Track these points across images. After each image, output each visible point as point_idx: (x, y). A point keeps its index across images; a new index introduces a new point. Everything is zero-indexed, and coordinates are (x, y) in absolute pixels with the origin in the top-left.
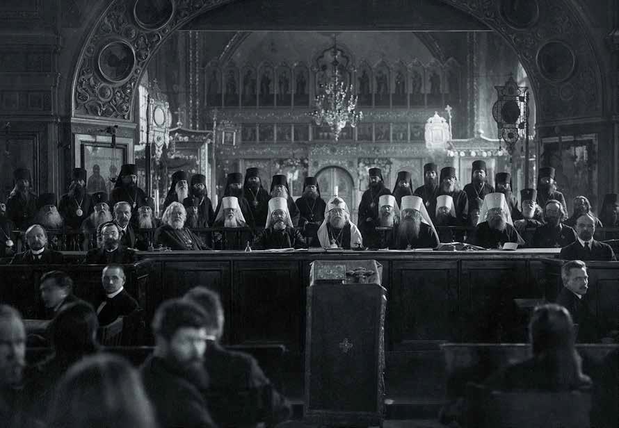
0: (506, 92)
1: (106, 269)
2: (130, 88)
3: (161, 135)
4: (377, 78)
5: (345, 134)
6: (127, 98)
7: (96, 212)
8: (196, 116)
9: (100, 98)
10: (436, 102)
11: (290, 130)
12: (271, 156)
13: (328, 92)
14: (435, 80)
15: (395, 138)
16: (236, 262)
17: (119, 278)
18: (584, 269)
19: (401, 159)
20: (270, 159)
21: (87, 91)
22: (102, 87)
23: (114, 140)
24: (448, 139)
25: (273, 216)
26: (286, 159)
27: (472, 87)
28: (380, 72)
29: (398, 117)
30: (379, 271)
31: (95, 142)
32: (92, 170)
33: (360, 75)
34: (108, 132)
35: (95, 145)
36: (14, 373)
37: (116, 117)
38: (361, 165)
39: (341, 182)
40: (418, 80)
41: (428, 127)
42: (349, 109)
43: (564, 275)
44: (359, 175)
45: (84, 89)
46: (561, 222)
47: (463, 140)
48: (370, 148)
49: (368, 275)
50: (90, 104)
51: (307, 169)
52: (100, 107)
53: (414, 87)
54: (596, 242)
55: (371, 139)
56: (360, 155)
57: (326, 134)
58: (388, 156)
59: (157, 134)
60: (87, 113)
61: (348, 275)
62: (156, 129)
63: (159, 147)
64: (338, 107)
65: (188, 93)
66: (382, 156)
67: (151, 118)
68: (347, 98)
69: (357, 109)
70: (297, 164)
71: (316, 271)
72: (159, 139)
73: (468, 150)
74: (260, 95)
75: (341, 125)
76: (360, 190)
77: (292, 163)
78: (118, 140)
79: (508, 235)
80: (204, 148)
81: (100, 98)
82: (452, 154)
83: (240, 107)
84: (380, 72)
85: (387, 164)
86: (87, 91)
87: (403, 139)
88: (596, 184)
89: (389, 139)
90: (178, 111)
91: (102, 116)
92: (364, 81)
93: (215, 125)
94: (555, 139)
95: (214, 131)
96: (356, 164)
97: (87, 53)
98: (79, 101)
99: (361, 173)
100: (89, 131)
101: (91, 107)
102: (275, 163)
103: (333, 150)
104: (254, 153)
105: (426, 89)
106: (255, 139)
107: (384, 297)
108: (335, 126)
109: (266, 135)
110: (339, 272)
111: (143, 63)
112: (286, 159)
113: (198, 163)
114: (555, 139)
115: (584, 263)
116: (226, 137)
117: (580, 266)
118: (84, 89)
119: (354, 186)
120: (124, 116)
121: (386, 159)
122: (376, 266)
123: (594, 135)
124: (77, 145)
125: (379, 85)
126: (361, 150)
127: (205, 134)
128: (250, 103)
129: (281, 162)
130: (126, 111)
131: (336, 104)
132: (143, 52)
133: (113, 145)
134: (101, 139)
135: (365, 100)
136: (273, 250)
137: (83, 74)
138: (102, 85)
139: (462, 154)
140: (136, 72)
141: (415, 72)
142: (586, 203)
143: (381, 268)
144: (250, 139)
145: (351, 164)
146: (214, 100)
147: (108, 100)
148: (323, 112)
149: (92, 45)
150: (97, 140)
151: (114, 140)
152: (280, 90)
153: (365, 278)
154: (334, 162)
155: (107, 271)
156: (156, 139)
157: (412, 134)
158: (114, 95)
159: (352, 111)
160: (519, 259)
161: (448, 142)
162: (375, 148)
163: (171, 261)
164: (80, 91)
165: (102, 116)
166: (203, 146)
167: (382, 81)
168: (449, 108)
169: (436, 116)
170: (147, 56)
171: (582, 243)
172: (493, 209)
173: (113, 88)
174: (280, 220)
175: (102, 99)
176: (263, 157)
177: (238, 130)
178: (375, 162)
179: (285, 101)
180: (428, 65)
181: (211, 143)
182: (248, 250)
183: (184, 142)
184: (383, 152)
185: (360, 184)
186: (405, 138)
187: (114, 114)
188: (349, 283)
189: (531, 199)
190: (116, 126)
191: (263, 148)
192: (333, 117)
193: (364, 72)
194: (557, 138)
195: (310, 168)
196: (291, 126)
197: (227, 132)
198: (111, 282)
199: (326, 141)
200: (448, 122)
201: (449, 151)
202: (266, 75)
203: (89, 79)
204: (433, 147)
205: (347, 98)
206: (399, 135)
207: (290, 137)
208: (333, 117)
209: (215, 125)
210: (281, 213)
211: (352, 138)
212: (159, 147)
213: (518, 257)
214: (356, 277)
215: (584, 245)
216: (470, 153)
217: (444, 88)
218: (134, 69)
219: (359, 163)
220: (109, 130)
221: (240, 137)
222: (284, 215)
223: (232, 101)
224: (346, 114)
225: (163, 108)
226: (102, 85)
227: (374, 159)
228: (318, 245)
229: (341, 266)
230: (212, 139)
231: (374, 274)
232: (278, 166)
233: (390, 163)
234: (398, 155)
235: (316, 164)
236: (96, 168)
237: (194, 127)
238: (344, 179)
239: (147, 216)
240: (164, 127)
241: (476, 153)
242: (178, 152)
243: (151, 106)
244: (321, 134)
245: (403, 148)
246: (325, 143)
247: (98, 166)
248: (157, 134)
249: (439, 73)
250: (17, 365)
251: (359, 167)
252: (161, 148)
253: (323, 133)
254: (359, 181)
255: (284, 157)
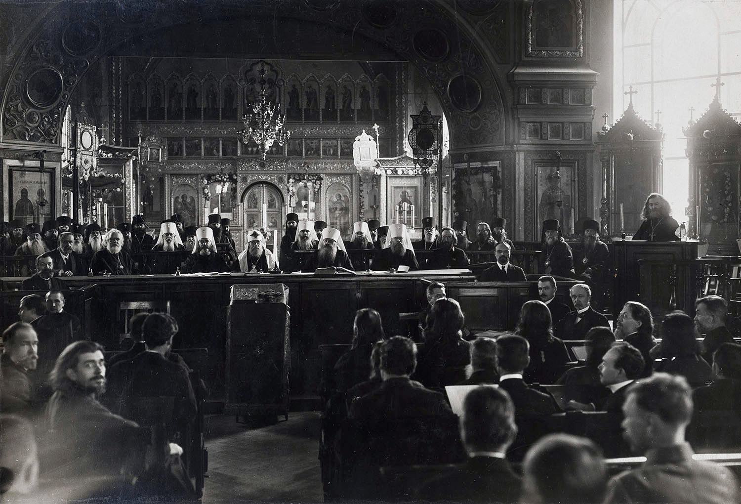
0: (420, 120)
1: (48, 294)
2: (58, 113)
3: (89, 158)
4: (307, 92)
5: (274, 149)
6: (55, 123)
7: (29, 241)
8: (119, 130)
9: (28, 123)
10: (366, 119)
11: (219, 144)
12: (198, 172)
13: (255, 111)
14: (365, 95)
15: (325, 152)
16: (16, 174)
17: (60, 301)
18: (443, 289)
19: (331, 175)
20: (197, 175)
21: (15, 117)
22: (30, 113)
23: (42, 164)
24: (376, 158)
25: (200, 243)
26: (214, 175)
27: (400, 102)
28: (310, 87)
29: (328, 133)
30: (286, 293)
31: (23, 167)
32: (20, 194)
33: (290, 89)
34: (36, 157)
35: (23, 169)
36: (32, 363)
37: (44, 141)
38: (291, 180)
39: (270, 198)
40: (348, 98)
41: (356, 145)
42: (277, 128)
43: (428, 294)
44: (288, 190)
45: (12, 115)
46: (454, 246)
47: (390, 159)
48: (299, 164)
49: (276, 295)
50: (18, 129)
51: (236, 185)
52: (28, 132)
53: (344, 103)
54: (511, 265)
55: (301, 154)
56: (290, 171)
57: (255, 149)
58: (318, 172)
59: (84, 158)
60: (15, 138)
61: (260, 296)
62: (83, 152)
63: (86, 170)
64: (266, 126)
65: (111, 106)
66: (313, 172)
67: (79, 142)
68: (275, 117)
69: (286, 126)
70: (225, 180)
71: (234, 294)
72: (86, 162)
73: (395, 168)
74: (186, 108)
75: (268, 144)
76: (290, 206)
77: (220, 179)
78: (46, 164)
79: (407, 259)
80: (129, 165)
81: (28, 123)
82: (378, 171)
83: (166, 120)
84: (310, 87)
85: (317, 180)
86: (15, 117)
87: (333, 154)
88: (500, 207)
89: (319, 155)
90: (101, 127)
91: (29, 140)
92: (294, 95)
93: (140, 141)
94: (464, 165)
95: (140, 148)
96: (285, 179)
97: (15, 80)
98: (7, 127)
99: (291, 189)
100: (17, 156)
101: (19, 132)
102: (202, 178)
103: (262, 165)
104: (180, 168)
105: (357, 104)
106: (181, 154)
107: (288, 312)
108: (263, 145)
109: (193, 150)
110: (253, 294)
111: (71, 88)
112: (214, 175)
113: (123, 181)
114: (464, 165)
115: (444, 285)
116: (151, 154)
117: (441, 287)
118: (12, 115)
119: (283, 201)
120: (52, 140)
121: (316, 174)
122: (284, 288)
123: (498, 162)
124: (6, 169)
125: (309, 100)
126: (292, 166)
127: (130, 151)
128: (175, 116)
129: (209, 177)
130: (54, 136)
131: (263, 123)
132: (71, 78)
133: (41, 169)
134: (28, 163)
135: (294, 115)
136: (200, 274)
137: (12, 100)
138: (30, 110)
139: (389, 172)
140: (64, 97)
141: (345, 87)
142: (488, 230)
143: (288, 291)
144: (177, 154)
145: (281, 180)
146: (140, 114)
147: (36, 125)
148: (251, 130)
149: (21, 72)
150: (25, 165)
151: (42, 164)
152: (208, 102)
153: (274, 298)
154: (264, 178)
155: (49, 296)
156: (83, 162)
157: (342, 149)
158: (42, 120)
159: (279, 130)
160: (408, 280)
161: (375, 160)
162: (305, 163)
163: (109, 285)
164: (8, 117)
165: (29, 140)
166: (128, 163)
167: (312, 97)
168: (376, 127)
169: (364, 134)
170: (74, 82)
171: (500, 266)
172: (396, 238)
173: (41, 113)
174: (205, 247)
175: (30, 124)
176: (190, 172)
177: (164, 146)
178: (306, 178)
179: (212, 115)
180: (358, 81)
181: (136, 159)
182: (178, 274)
183: (107, 159)
184: (313, 168)
185: (290, 200)
186: (335, 153)
187: (41, 139)
188: (261, 302)
189: (431, 226)
190: (45, 151)
191: (189, 164)
192: (260, 136)
193: (294, 86)
194: (466, 164)
195: (239, 184)
196: (219, 141)
197: (151, 148)
198: (54, 305)
199: (254, 156)
200: (375, 140)
201: (376, 169)
202: (193, 88)
203: (17, 106)
204: (360, 164)
205: (275, 117)
206: (329, 150)
207: (218, 151)
208: (260, 136)
209: (140, 141)
210: (207, 241)
211: (282, 154)
212: (86, 170)
213: (407, 278)
214: (266, 298)
215: (501, 269)
216: (396, 172)
217: (374, 105)
218: (61, 94)
219: (289, 179)
220: (38, 155)
221: (166, 153)
222: (209, 244)
223: (157, 115)
224: (274, 133)
225: (91, 131)
226: (30, 110)
227: (304, 175)
228: (238, 270)
229: (255, 289)
230: (137, 156)
231: (281, 294)
232: (206, 182)
233: (320, 179)
234: (329, 171)
235: (244, 179)
236: (24, 192)
237: (117, 143)
238: (274, 196)
239: (78, 242)
240: (92, 150)
241: (403, 172)
242: (102, 169)
243: (79, 130)
244: (250, 149)
245: (333, 164)
246: (254, 158)
247: (26, 190)
248: (84, 158)
249: (369, 88)
250: (34, 357)
251: (288, 182)
252: (88, 171)
253: (253, 152)
254: (289, 197)
255: (210, 172)
